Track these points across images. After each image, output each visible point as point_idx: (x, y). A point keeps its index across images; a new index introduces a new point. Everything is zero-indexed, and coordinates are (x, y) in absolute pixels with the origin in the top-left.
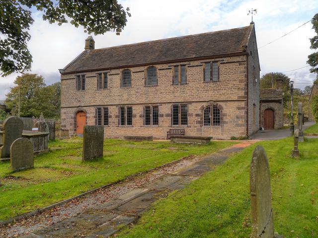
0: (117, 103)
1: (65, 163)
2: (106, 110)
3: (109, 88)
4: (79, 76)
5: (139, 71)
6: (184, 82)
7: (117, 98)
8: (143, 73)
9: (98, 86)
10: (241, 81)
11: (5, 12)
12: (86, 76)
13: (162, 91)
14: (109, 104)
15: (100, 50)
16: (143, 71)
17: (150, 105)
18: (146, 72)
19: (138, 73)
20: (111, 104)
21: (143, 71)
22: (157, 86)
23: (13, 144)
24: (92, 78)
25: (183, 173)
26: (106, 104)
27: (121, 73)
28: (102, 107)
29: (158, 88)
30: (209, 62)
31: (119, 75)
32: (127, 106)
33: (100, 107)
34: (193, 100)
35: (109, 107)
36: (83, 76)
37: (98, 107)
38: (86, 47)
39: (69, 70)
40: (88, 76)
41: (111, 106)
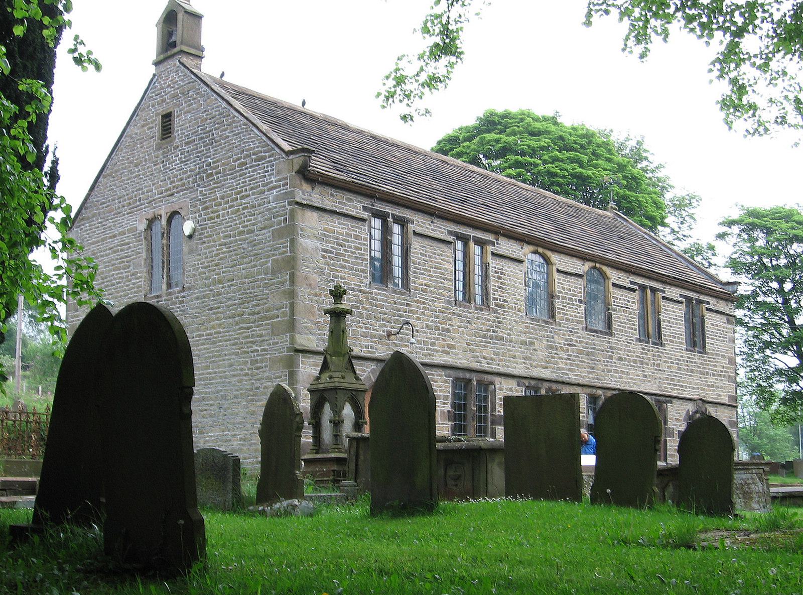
0: (519, 370)
1: (311, 515)
2: (485, 386)
5: (574, 271)
7: (519, 351)
10: (101, 182)
14: (494, 368)
15: (121, 313)
16: (581, 276)
17: (600, 392)
19: (569, 278)
20: (502, 370)
21: (581, 276)
23: (14, 479)
24: (435, 244)
26: (485, 366)
28: (475, 378)
29: (613, 340)
30: (485, 267)
32: (546, 385)
33: (468, 375)
34: (674, 393)
35: (497, 380)
37: (461, 375)
40: (419, 230)
41: (502, 380)
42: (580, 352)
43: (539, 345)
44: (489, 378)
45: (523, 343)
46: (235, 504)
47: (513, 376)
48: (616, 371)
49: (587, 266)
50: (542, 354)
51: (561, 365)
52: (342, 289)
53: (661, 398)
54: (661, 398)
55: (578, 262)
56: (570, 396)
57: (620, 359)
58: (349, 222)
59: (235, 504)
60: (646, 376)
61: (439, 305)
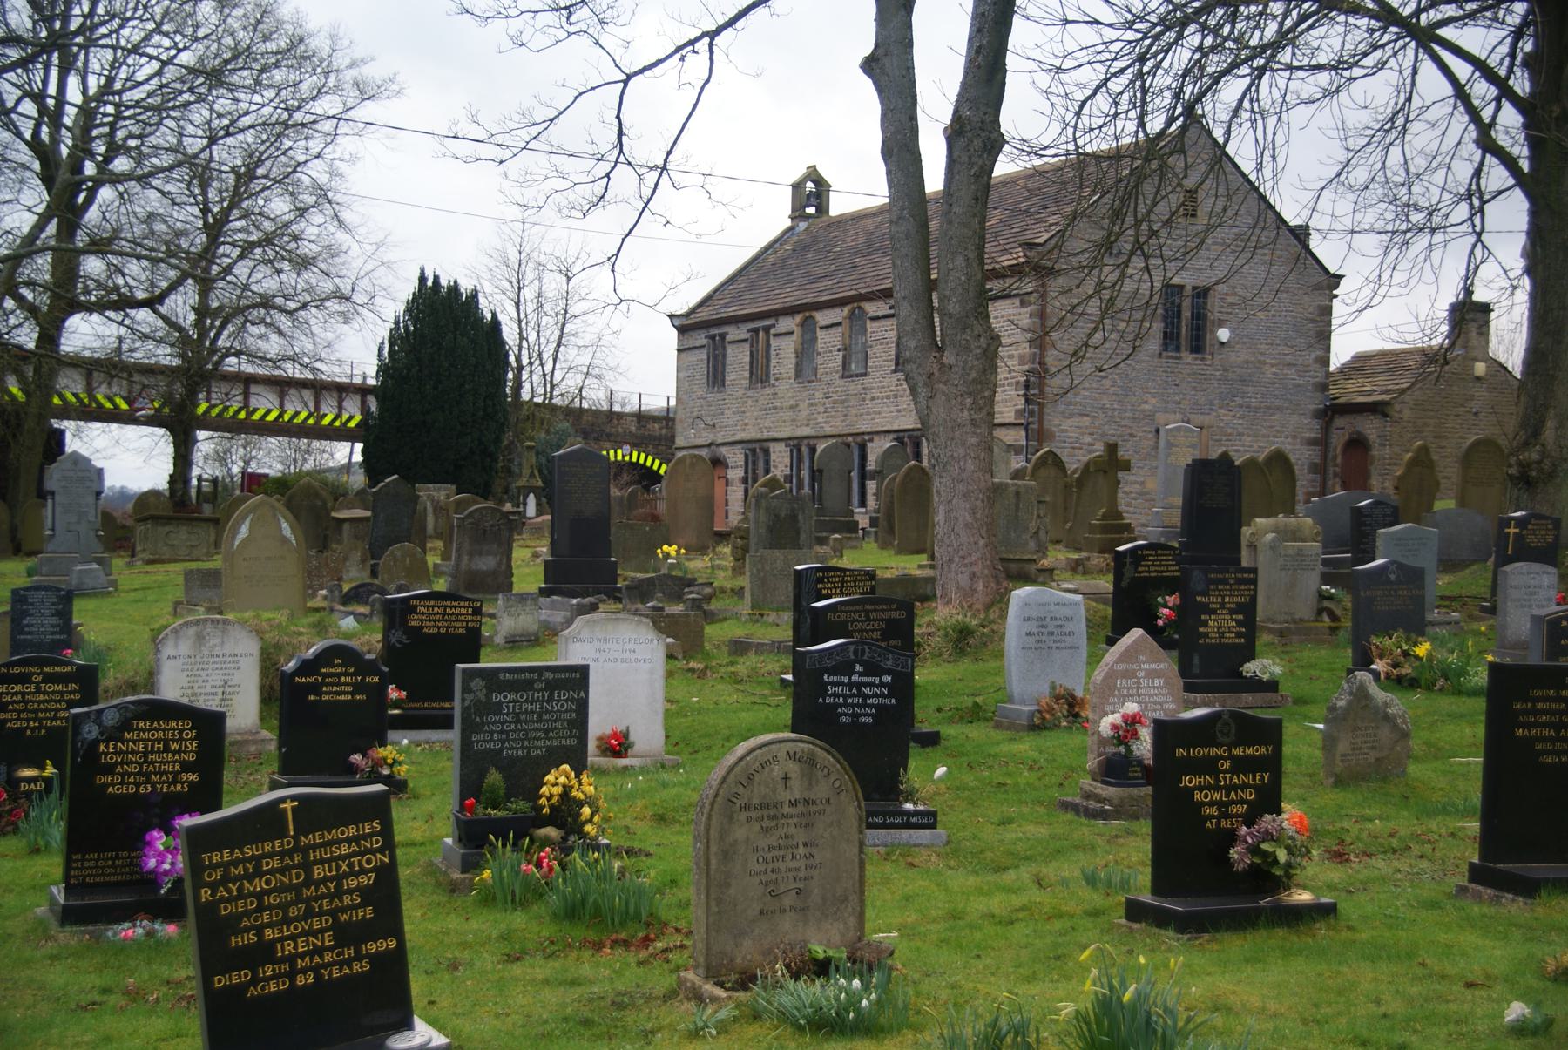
3: (772, 381)
4: (713, 337)
5: (830, 322)
6: (1310, 472)
7: (788, 415)
8: (840, 329)
9: (751, 373)
11: (1534, 705)
12: (728, 338)
13: (875, 393)
16: (839, 324)
17: (850, 439)
18: (846, 324)
22: (865, 374)
25: (514, 636)
27: (797, 330)
28: (757, 446)
29: (867, 380)
31: (794, 337)
32: (806, 442)
35: (771, 445)
36: (723, 336)
37: (750, 446)
38: (793, 210)
39: (703, 315)
42: (835, 402)
43: (803, 406)
44: (765, 444)
45: (791, 407)
46: (10, 439)
47: (781, 440)
48: (868, 414)
49: (846, 310)
50: (804, 413)
51: (820, 420)
52: (889, 962)
53: (915, 433)
54: (915, 433)
55: (837, 310)
56: (962, 142)
57: (873, 399)
58: (697, 351)
59: (10, 439)
60: (899, 411)
61: (740, 393)
